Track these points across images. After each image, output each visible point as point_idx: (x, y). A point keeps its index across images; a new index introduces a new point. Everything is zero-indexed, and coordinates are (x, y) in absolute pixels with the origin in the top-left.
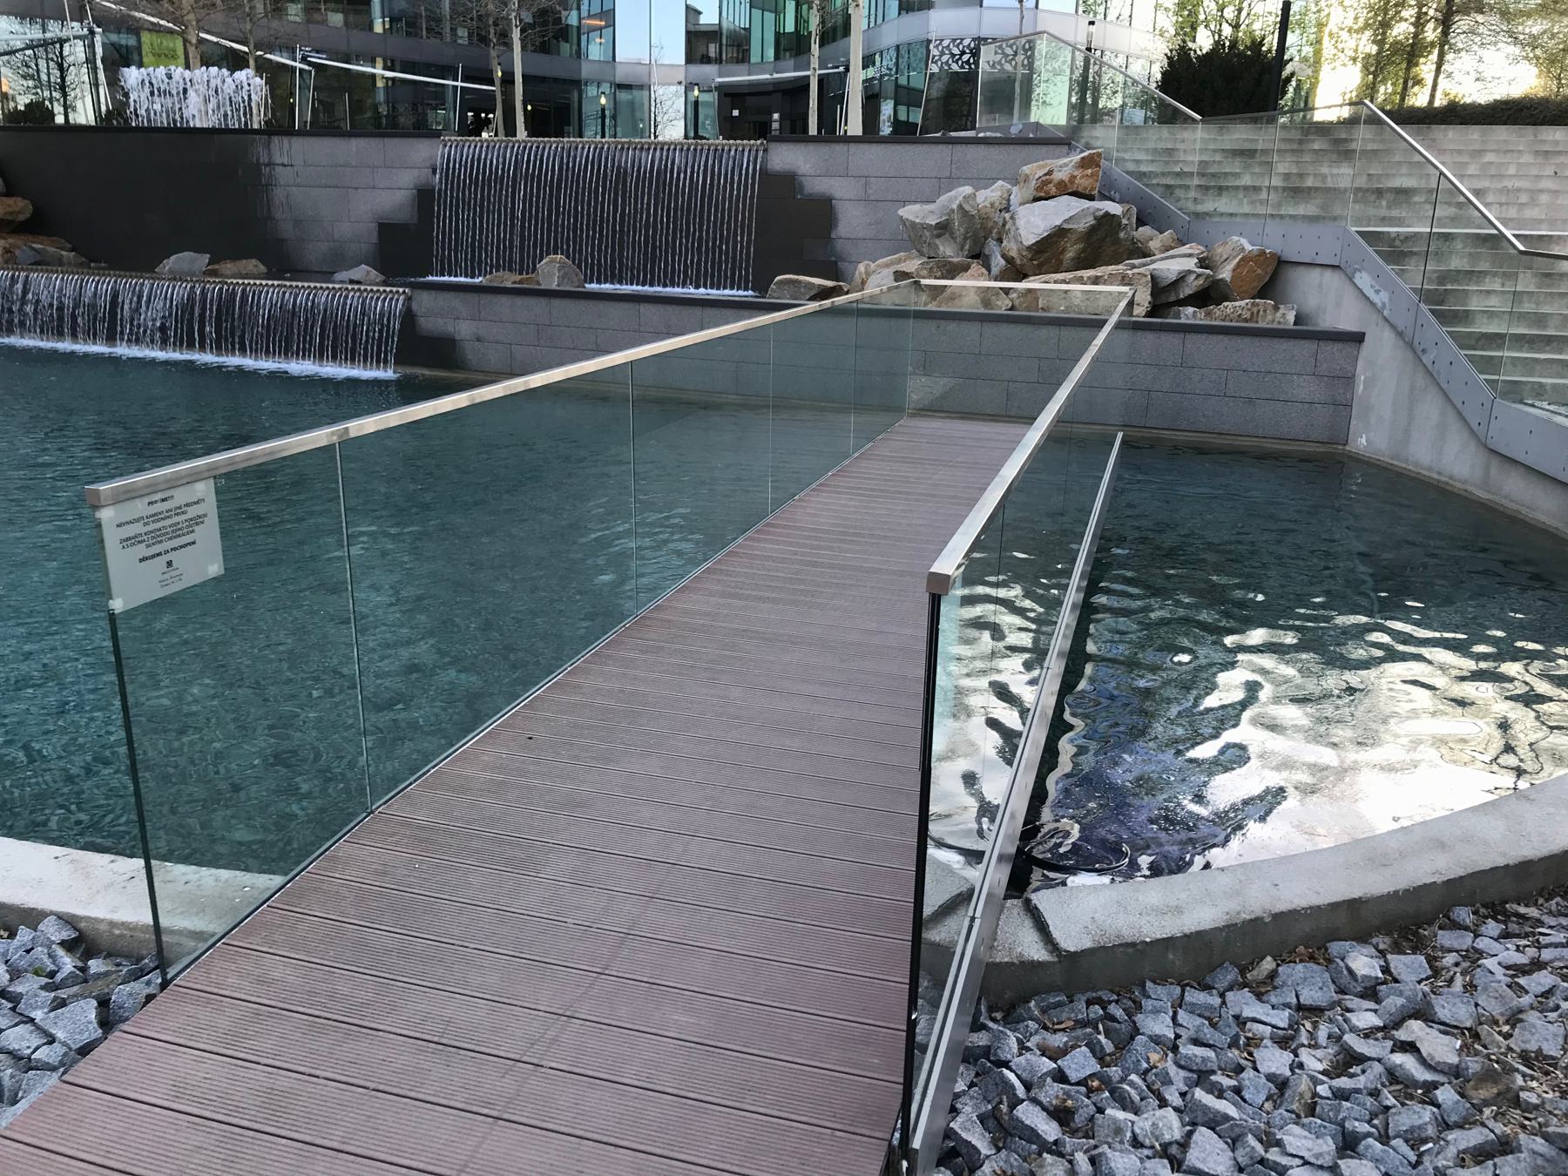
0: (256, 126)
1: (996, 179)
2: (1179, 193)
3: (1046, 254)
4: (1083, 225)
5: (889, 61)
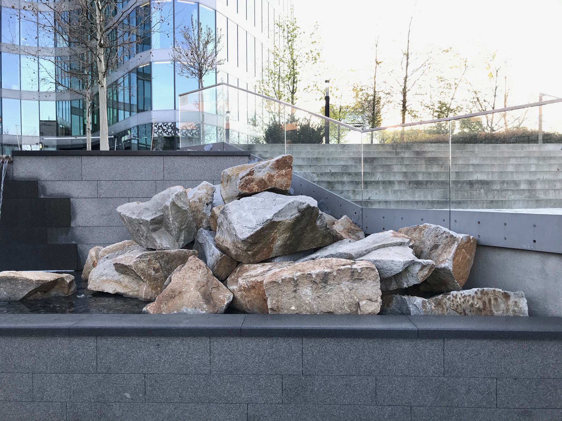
1: (199, 181)
2: (339, 187)
3: (260, 247)
4: (289, 217)
5: (134, 133)
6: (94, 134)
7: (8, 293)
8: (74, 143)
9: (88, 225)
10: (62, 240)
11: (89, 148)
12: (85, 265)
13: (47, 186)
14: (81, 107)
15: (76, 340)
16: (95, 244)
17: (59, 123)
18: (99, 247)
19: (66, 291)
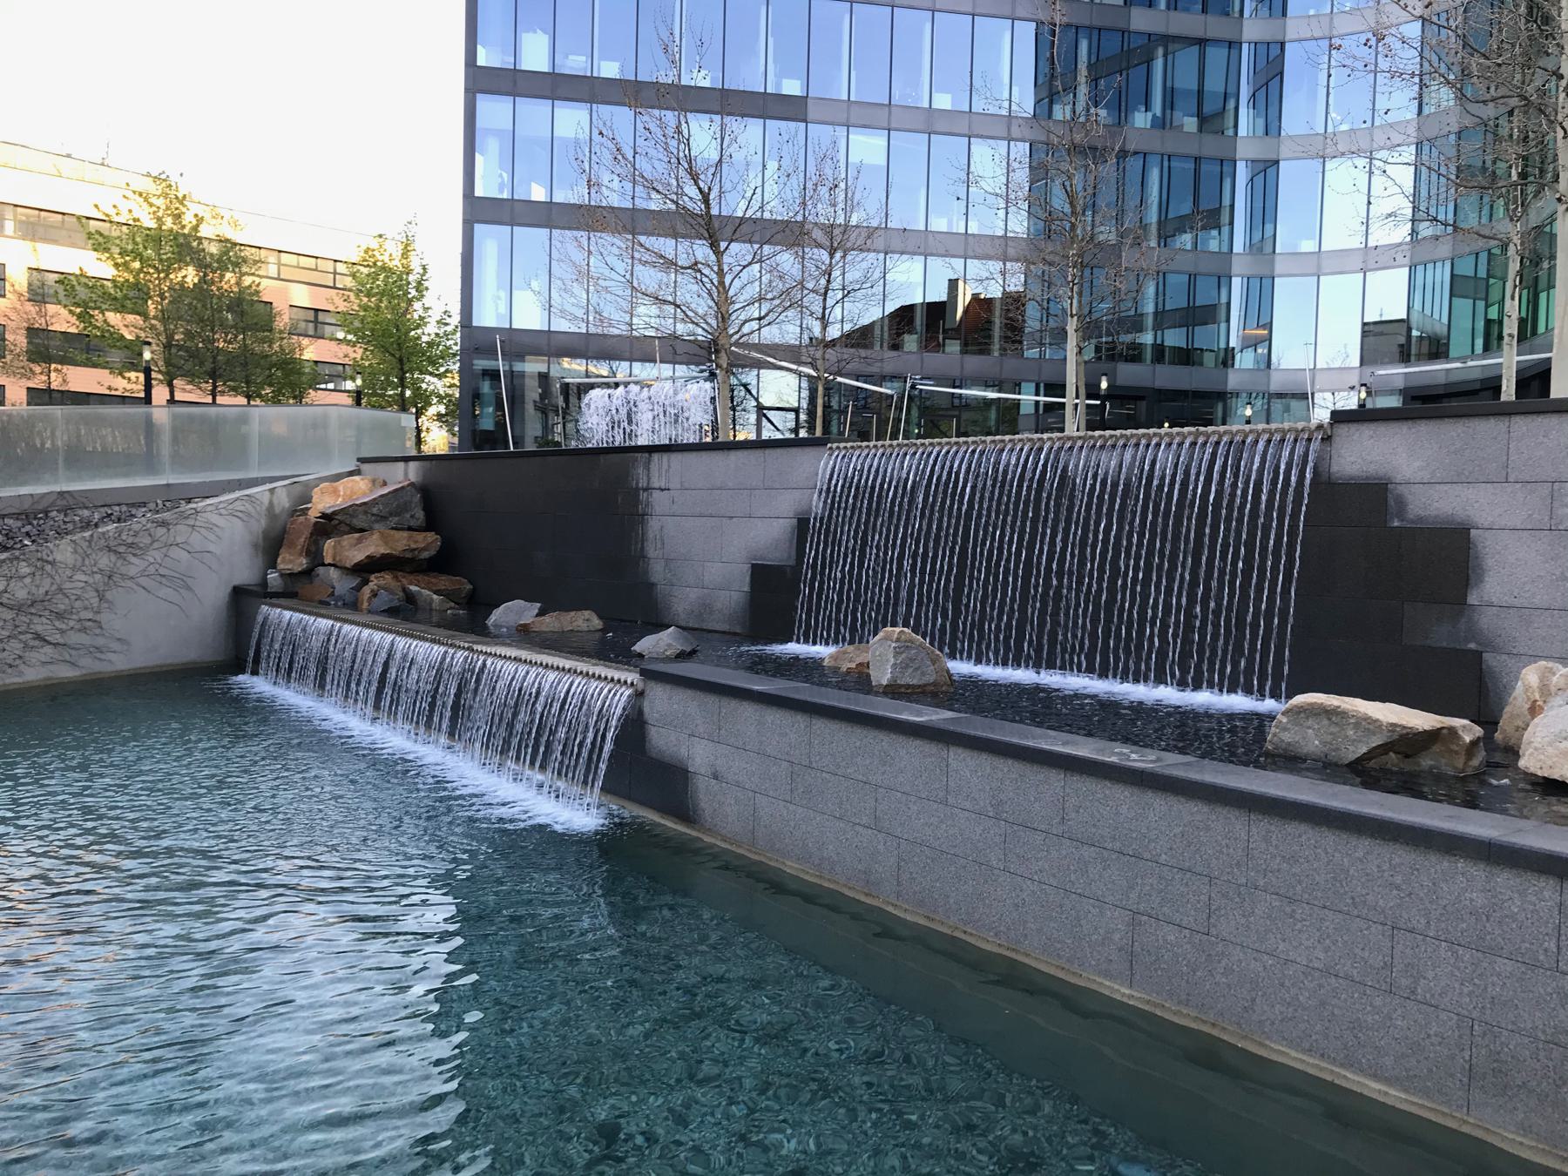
0: (530, 446)
6: (1526, 345)
7: (1324, 743)
8: (1454, 378)
9: (1517, 602)
10: (1441, 636)
11: (1508, 391)
12: (1507, 709)
13: (1410, 498)
14: (1482, 273)
15: (1505, 875)
16: (1536, 658)
17: (1414, 324)
18: (1550, 664)
19: (1460, 763)
